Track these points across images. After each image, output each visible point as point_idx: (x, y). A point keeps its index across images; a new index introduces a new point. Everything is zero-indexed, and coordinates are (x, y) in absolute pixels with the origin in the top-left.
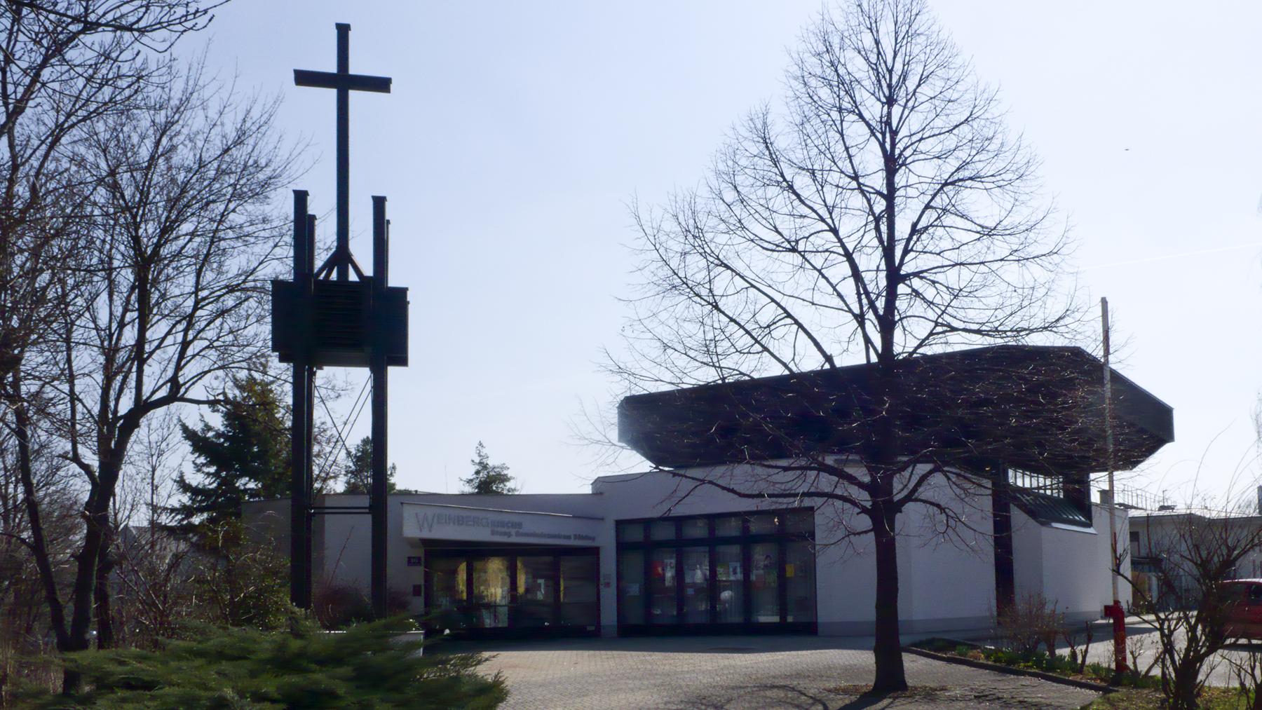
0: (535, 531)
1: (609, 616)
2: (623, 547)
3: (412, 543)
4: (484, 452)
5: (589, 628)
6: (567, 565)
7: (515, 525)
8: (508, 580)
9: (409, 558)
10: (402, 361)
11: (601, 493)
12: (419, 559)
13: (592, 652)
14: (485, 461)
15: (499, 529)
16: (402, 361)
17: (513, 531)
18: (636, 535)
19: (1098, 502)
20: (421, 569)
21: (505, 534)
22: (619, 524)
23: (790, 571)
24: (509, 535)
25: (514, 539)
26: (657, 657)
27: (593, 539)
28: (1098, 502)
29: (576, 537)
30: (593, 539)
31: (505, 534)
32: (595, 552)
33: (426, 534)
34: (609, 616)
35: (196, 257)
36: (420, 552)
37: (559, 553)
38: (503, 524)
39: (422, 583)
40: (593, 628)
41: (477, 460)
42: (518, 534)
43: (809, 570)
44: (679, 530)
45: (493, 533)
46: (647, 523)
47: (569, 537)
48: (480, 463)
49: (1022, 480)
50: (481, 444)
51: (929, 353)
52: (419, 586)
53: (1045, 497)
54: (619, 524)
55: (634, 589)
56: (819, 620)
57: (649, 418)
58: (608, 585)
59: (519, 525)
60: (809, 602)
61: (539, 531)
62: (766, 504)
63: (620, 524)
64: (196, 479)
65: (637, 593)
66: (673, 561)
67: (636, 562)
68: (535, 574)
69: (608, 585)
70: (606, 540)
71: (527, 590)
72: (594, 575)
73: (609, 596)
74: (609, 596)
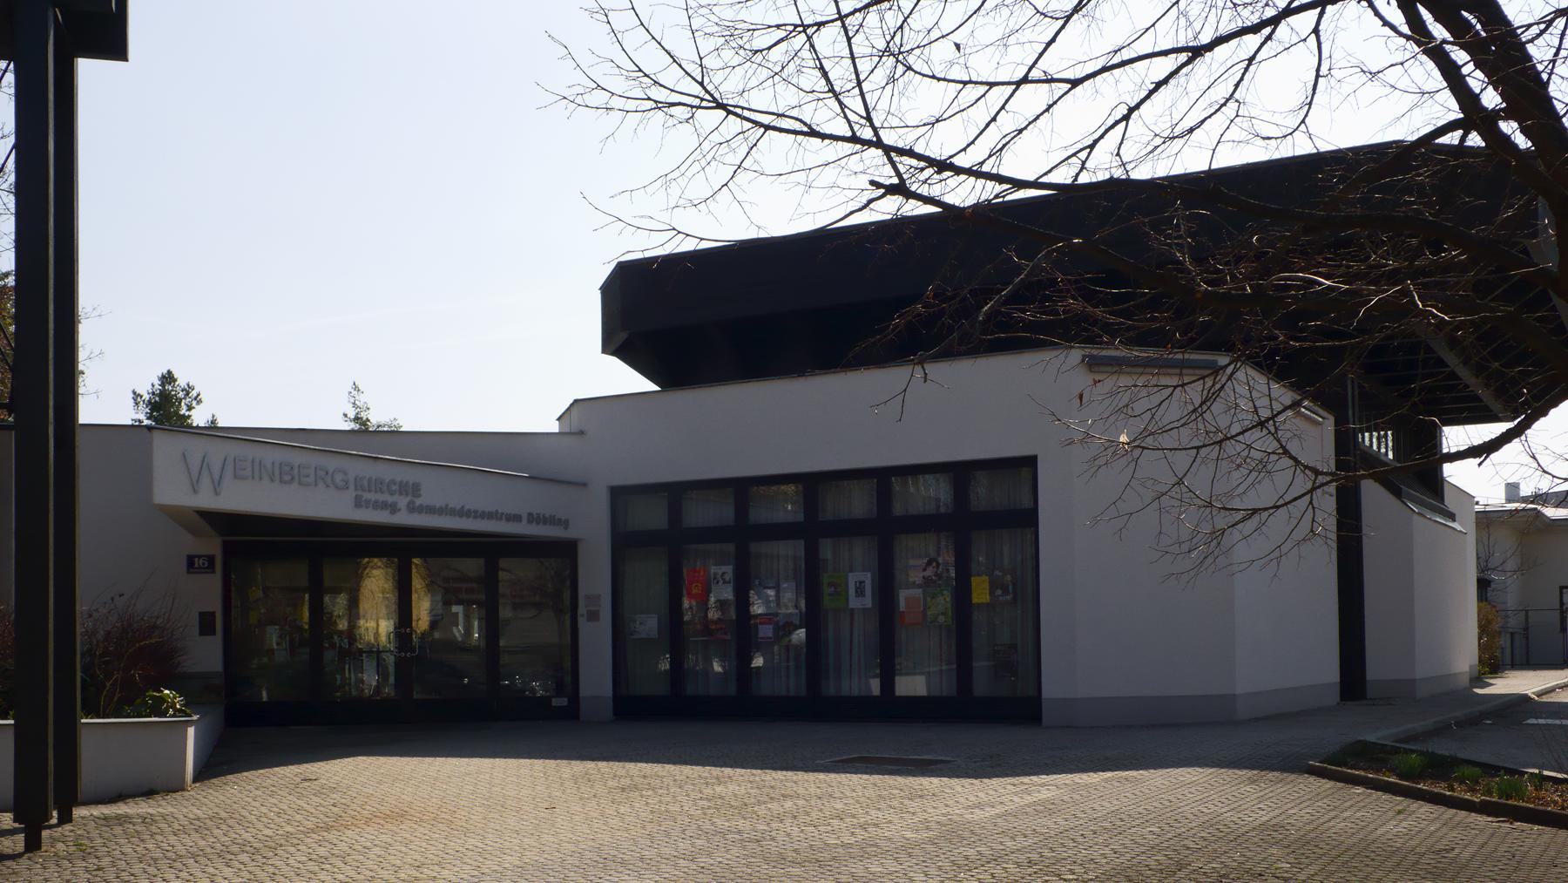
0: (443, 504)
1: (596, 679)
2: (625, 543)
3: (175, 514)
4: (362, 400)
6: (514, 571)
7: (404, 488)
8: (393, 597)
10: (113, 45)
11: (582, 433)
12: (211, 559)
13: (578, 766)
14: (364, 415)
15: (372, 496)
16: (113, 45)
17: (402, 502)
18: (653, 517)
20: (214, 582)
21: (384, 506)
23: (980, 592)
24: (394, 509)
25: (403, 519)
26: (737, 783)
27: (565, 524)
29: (532, 519)
31: (384, 506)
32: (565, 551)
33: (206, 500)
34: (596, 679)
36: (212, 546)
37: (491, 549)
38: (378, 485)
40: (563, 702)
41: (352, 415)
42: (412, 509)
43: (1024, 590)
44: (742, 509)
45: (358, 503)
46: (676, 493)
47: (517, 518)
48: (357, 419)
49: (1370, 440)
50: (356, 388)
51: (1453, 55)
52: (213, 614)
55: (648, 625)
56: (1045, 694)
57: (673, 312)
58: (593, 616)
59: (415, 490)
60: (1023, 656)
61: (455, 504)
63: (620, 496)
64: (383, 639)
65: (654, 634)
66: (728, 570)
67: (650, 575)
68: (449, 593)
69: (593, 616)
70: (592, 528)
71: (434, 625)
72: (562, 595)
73: (596, 640)
74: (596, 640)
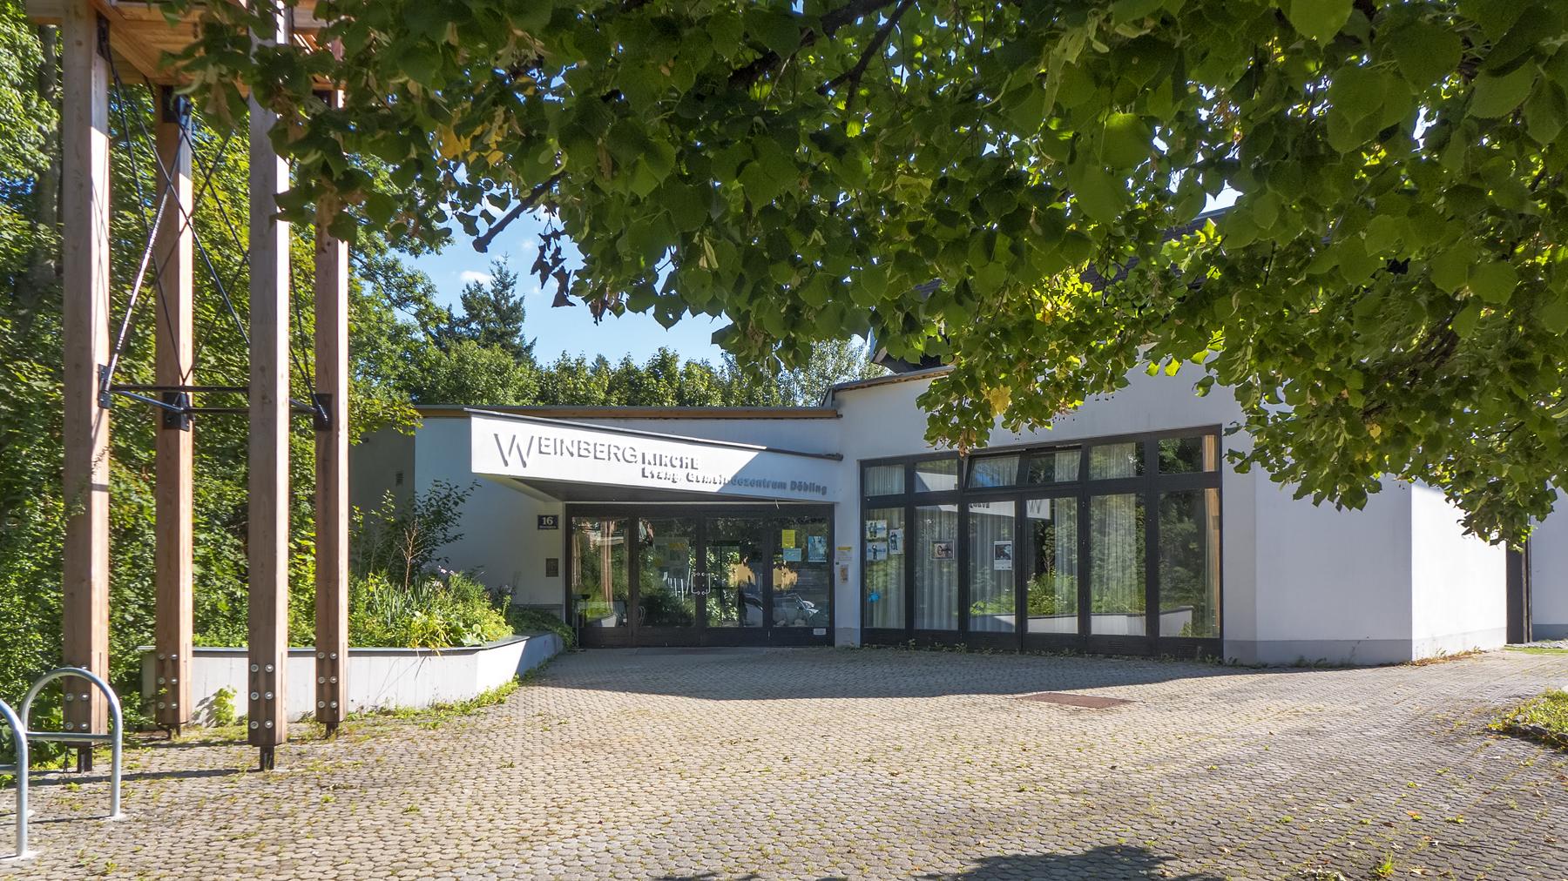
2: (871, 505)
5: (816, 632)
9: (540, 519)
12: (555, 518)
18: (895, 483)
19: (279, 223)
22: (865, 465)
27: (824, 491)
28: (279, 223)
29: (795, 486)
30: (824, 491)
35: (1070, 606)
36: (558, 508)
39: (346, 663)
40: (823, 632)
44: (910, 479)
47: (782, 486)
53: (701, 168)
54: (865, 465)
62: (1212, 532)
